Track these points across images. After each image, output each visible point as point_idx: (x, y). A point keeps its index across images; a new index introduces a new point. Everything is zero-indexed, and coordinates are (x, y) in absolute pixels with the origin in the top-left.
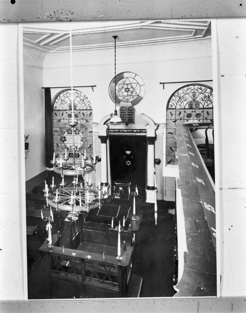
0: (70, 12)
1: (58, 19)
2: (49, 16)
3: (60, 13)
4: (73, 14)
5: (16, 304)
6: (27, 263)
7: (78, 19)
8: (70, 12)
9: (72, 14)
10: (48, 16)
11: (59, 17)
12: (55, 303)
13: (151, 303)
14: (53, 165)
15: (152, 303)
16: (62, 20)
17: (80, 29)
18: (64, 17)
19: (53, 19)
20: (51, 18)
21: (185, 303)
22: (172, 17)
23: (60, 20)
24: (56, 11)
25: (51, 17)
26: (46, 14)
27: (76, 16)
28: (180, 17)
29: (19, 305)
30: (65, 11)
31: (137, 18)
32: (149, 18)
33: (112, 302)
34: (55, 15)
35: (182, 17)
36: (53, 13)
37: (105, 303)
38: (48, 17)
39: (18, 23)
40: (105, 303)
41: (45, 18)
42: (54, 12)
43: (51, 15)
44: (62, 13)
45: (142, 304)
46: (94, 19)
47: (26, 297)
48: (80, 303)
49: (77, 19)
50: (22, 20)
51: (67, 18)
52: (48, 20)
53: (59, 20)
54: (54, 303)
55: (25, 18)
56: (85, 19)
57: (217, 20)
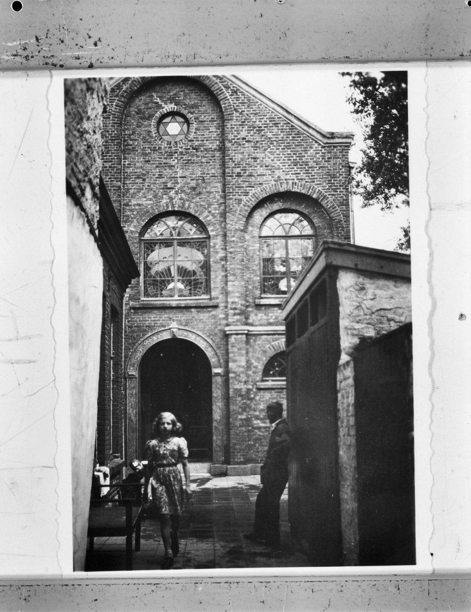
0: (90, 37)
1: (50, 61)
2: (21, 52)
3: (54, 40)
4: (98, 43)
6: (415, 445)
7: (116, 62)
8: (90, 37)
9: (96, 44)
11: (53, 56)
12: (70, 587)
15: (392, 589)
16: (62, 66)
17: (265, 96)
18: (70, 54)
19: (32, 62)
22: (428, 56)
24: (42, 35)
25: (25, 53)
26: (10, 44)
27: (109, 49)
30: (73, 35)
31: (311, 58)
32: (352, 57)
33: (257, 585)
34: (39, 48)
35: (462, 55)
36: (34, 40)
37: (234, 586)
38: (15, 55)
40: (234, 586)
41: (6, 58)
42: (37, 39)
43: (25, 49)
45: (360, 591)
46: (170, 61)
48: (154, 588)
49: (111, 62)
52: (18, 65)
54: (65, 587)
56: (140, 60)
57: (429, 69)
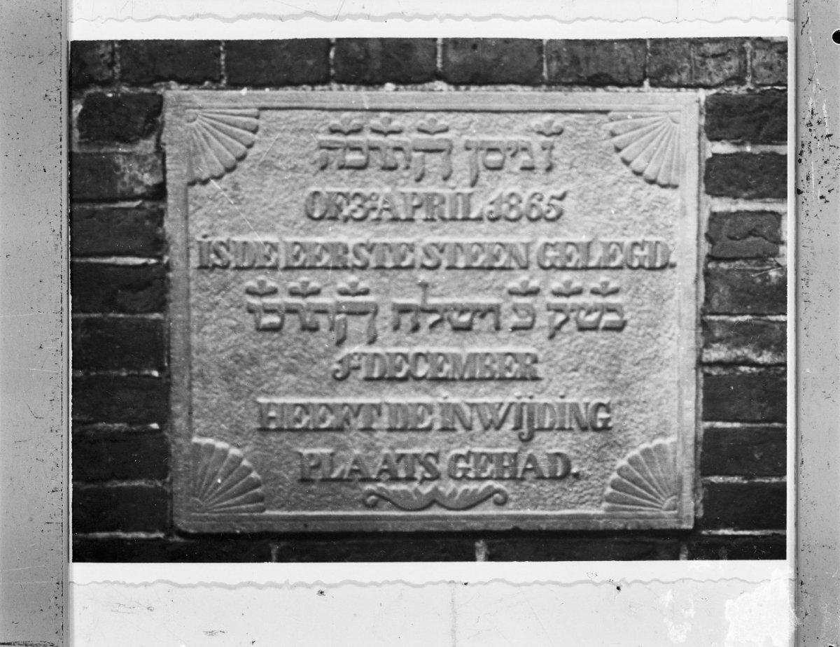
1: (805, 149)
2: (816, 118)
3: (827, 155)
4: (823, 200)
5: (58, 6)
8: (829, 191)
9: (822, 197)
10: (815, 112)
13: (54, 481)
14: (87, 540)
15: (54, 484)
16: (800, 161)
18: (813, 169)
20: (810, 124)
21: (53, 600)
22: (801, 547)
23: (801, 154)
25: (814, 123)
26: (824, 106)
27: (816, 211)
28: (801, 574)
29: (53, 17)
34: (819, 138)
36: (828, 132)
39: (796, 20)
41: (810, 103)
42: (829, 136)
43: (819, 123)
44: (826, 162)
45: (51, 450)
46: (803, 275)
47: (80, 31)
48: (57, 232)
50: (805, 20)
51: (808, 178)
52: (802, 115)
53: (802, 152)
55: (810, 32)
